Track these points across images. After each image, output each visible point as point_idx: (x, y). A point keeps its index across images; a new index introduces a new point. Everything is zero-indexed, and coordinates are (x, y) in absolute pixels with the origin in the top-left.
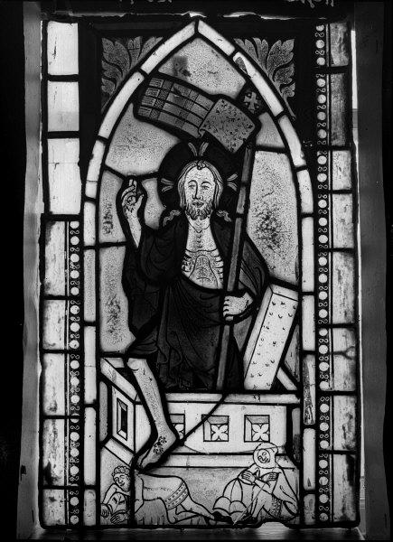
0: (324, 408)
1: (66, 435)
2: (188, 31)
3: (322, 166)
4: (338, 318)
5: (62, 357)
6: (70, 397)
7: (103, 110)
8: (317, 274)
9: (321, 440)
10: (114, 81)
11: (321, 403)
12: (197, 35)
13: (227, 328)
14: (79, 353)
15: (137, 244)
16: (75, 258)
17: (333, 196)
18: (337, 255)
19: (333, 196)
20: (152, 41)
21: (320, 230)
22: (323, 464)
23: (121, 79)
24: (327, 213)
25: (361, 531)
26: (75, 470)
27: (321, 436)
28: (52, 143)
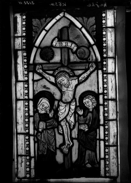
0: (107, 150)
1: (23, 67)
2: (62, 15)
3: (104, 23)
4: (111, 143)
5: (23, 136)
6: (26, 162)
7: (34, 41)
8: (103, 84)
9: (105, 90)
10: (37, 32)
11: (106, 155)
12: (64, 16)
13: (78, 104)
14: (27, 82)
15: (49, 180)
16: (27, 120)
17: (108, 59)
18: (110, 102)
19: (108, 59)
20: (49, 19)
21: (106, 135)
22: (107, 150)
23: (40, 32)
24: (107, 106)
25: (119, 180)
26: (27, 149)
27: (106, 130)
28: (18, 136)
